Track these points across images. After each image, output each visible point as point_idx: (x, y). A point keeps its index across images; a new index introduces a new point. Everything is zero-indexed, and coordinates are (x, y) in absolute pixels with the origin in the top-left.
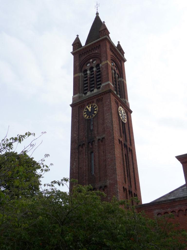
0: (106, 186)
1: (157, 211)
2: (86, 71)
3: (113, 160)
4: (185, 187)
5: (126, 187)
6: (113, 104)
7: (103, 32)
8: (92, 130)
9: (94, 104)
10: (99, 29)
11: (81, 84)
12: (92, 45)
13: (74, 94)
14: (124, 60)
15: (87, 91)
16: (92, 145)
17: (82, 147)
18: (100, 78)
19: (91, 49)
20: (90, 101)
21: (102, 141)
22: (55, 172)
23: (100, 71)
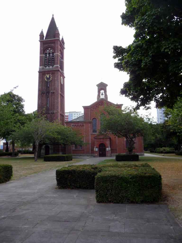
0: (54, 113)
1: (72, 124)
2: (46, 54)
3: (58, 103)
4: (83, 116)
5: (61, 113)
6: (59, 76)
7: (57, 34)
8: (49, 87)
9: (50, 75)
10: (53, 28)
11: (43, 61)
12: (51, 40)
13: (40, 66)
14: (64, 48)
15: (46, 66)
16: (48, 94)
17: (44, 94)
18: (53, 60)
19: (50, 42)
20: (48, 72)
21: (53, 94)
22: (30, 106)
23: (54, 57)
